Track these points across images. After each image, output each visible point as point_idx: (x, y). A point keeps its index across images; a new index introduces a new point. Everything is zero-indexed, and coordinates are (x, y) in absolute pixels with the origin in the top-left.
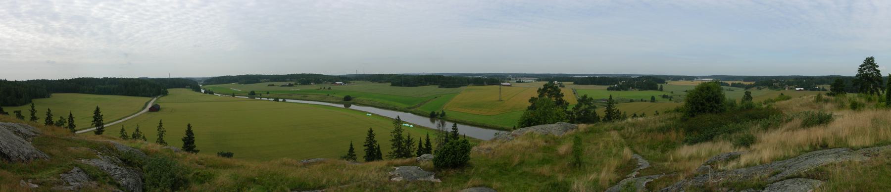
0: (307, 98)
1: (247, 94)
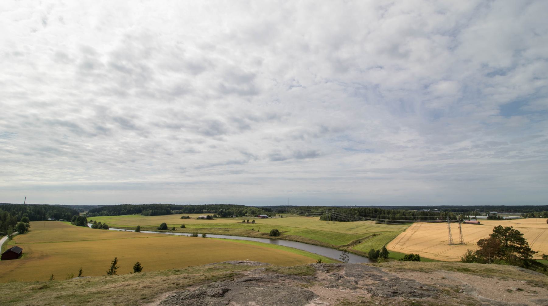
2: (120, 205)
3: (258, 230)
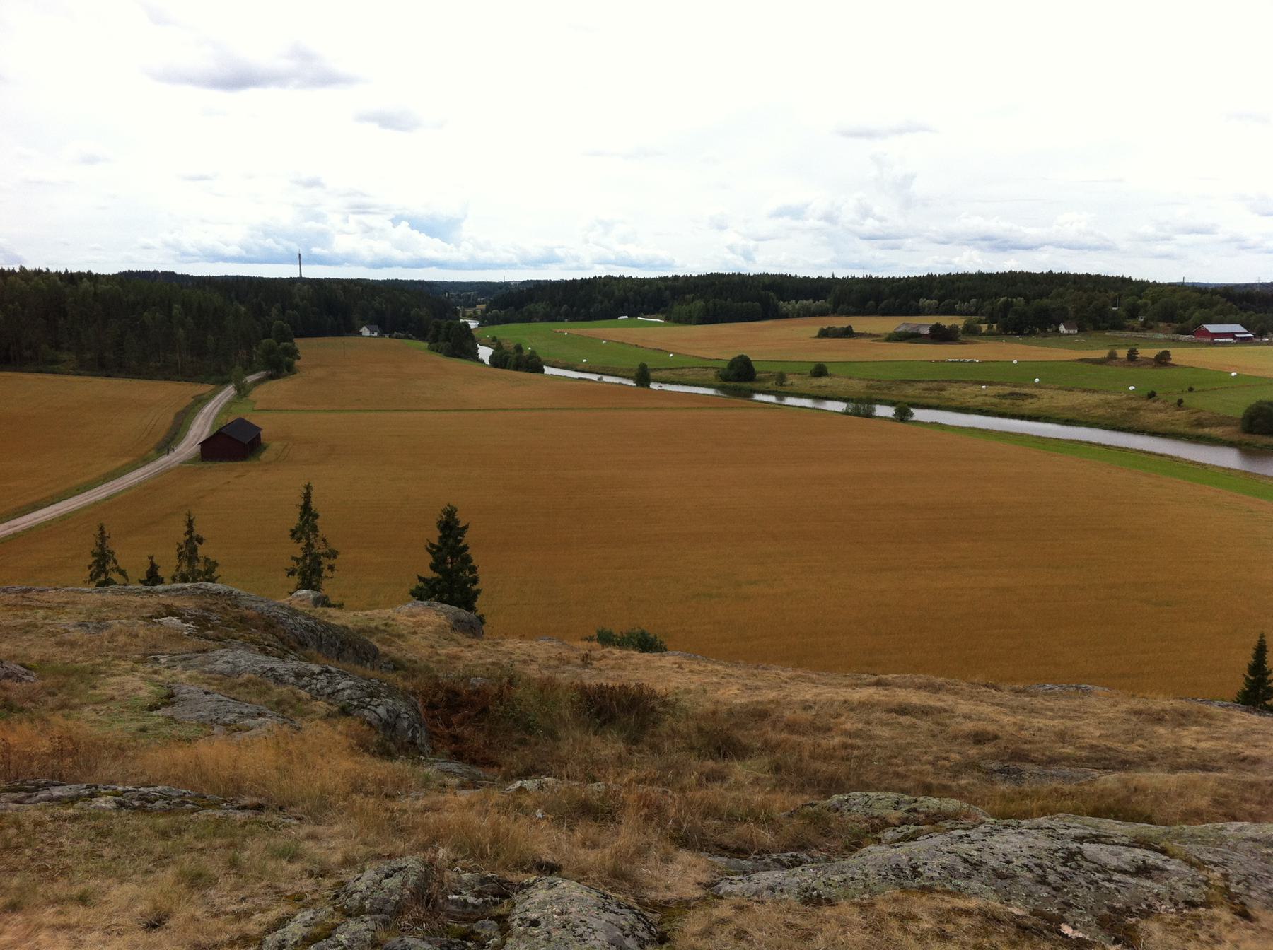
0: (1029, 406)
1: (711, 374)
2: (589, 279)
3: (1180, 402)
